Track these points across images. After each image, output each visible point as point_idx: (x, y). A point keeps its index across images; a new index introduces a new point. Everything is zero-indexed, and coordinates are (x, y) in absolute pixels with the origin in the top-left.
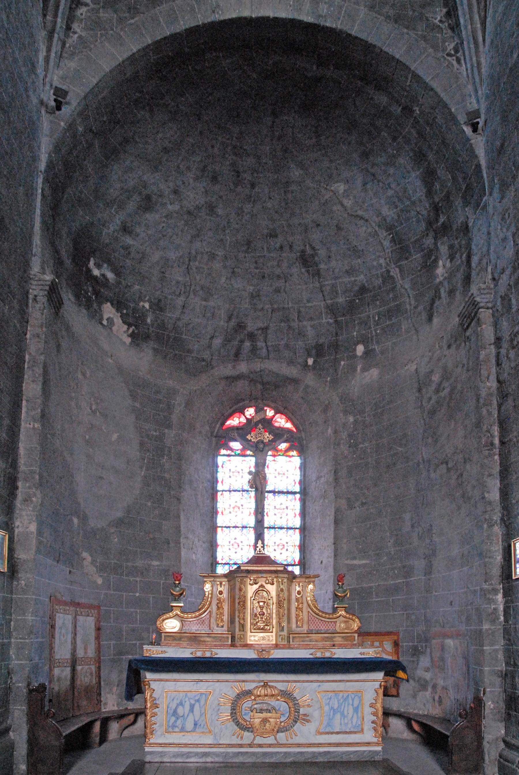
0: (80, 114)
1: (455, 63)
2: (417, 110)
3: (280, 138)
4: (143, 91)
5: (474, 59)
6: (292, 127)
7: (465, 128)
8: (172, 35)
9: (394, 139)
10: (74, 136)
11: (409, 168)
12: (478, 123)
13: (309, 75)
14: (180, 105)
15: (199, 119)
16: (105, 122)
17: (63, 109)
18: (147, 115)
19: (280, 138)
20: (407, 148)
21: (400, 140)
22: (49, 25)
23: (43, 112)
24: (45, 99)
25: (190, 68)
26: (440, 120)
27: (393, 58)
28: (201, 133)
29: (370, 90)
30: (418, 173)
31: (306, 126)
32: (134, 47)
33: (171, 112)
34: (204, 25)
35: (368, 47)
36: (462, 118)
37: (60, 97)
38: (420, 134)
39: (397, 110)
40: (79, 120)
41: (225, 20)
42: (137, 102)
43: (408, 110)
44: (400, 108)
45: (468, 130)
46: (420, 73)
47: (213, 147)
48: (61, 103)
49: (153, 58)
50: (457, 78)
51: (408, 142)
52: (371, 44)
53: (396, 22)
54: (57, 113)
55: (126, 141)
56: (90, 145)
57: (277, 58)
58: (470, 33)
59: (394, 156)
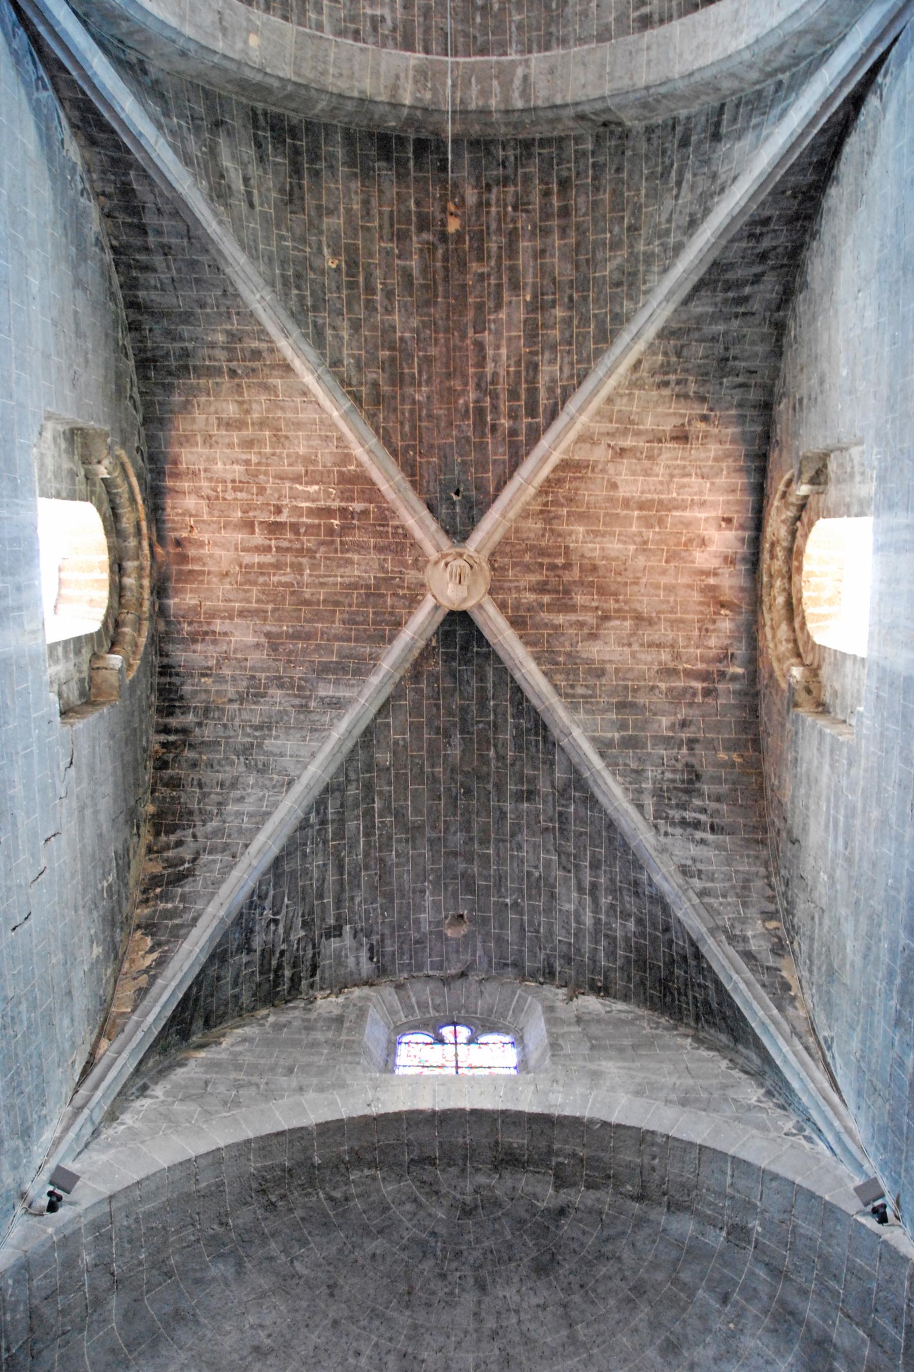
0: (95, 1226)
1: (803, 1142)
2: (756, 1225)
3: (494, 1335)
4: (227, 1224)
5: (836, 1123)
6: (517, 1312)
7: (862, 1220)
8: (292, 1131)
9: (725, 1299)
10: (70, 1263)
11: (770, 1353)
12: (884, 1206)
13: (542, 1205)
14: (296, 1263)
15: (332, 1295)
16: (140, 1264)
17: (61, 1211)
18: (230, 1273)
19: (494, 1335)
20: (753, 1310)
21: (735, 1296)
22: (79, 1099)
23: (19, 1210)
24: (32, 1193)
25: (322, 1195)
26: (807, 1228)
27: (691, 1144)
28: (335, 1323)
29: (659, 1216)
30: (790, 1359)
31: (544, 1307)
32: (220, 1135)
33: (278, 1274)
34: (351, 1119)
35: (643, 1138)
36: (852, 1206)
37: (62, 1184)
38: (776, 1272)
39: (717, 1239)
40: (87, 1239)
41: (386, 1114)
42: (214, 1240)
43: (738, 1233)
44: (724, 1234)
45: (871, 1223)
46: (743, 1155)
47: (358, 1354)
48: (60, 1198)
49: (254, 1165)
50: (818, 1160)
51: (751, 1295)
52: (647, 1131)
53: (683, 1105)
54: (48, 1215)
55: (179, 1316)
56: (98, 1302)
57: (482, 1179)
58: (815, 1092)
59: (732, 1335)
